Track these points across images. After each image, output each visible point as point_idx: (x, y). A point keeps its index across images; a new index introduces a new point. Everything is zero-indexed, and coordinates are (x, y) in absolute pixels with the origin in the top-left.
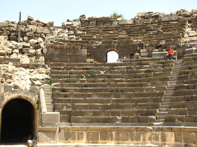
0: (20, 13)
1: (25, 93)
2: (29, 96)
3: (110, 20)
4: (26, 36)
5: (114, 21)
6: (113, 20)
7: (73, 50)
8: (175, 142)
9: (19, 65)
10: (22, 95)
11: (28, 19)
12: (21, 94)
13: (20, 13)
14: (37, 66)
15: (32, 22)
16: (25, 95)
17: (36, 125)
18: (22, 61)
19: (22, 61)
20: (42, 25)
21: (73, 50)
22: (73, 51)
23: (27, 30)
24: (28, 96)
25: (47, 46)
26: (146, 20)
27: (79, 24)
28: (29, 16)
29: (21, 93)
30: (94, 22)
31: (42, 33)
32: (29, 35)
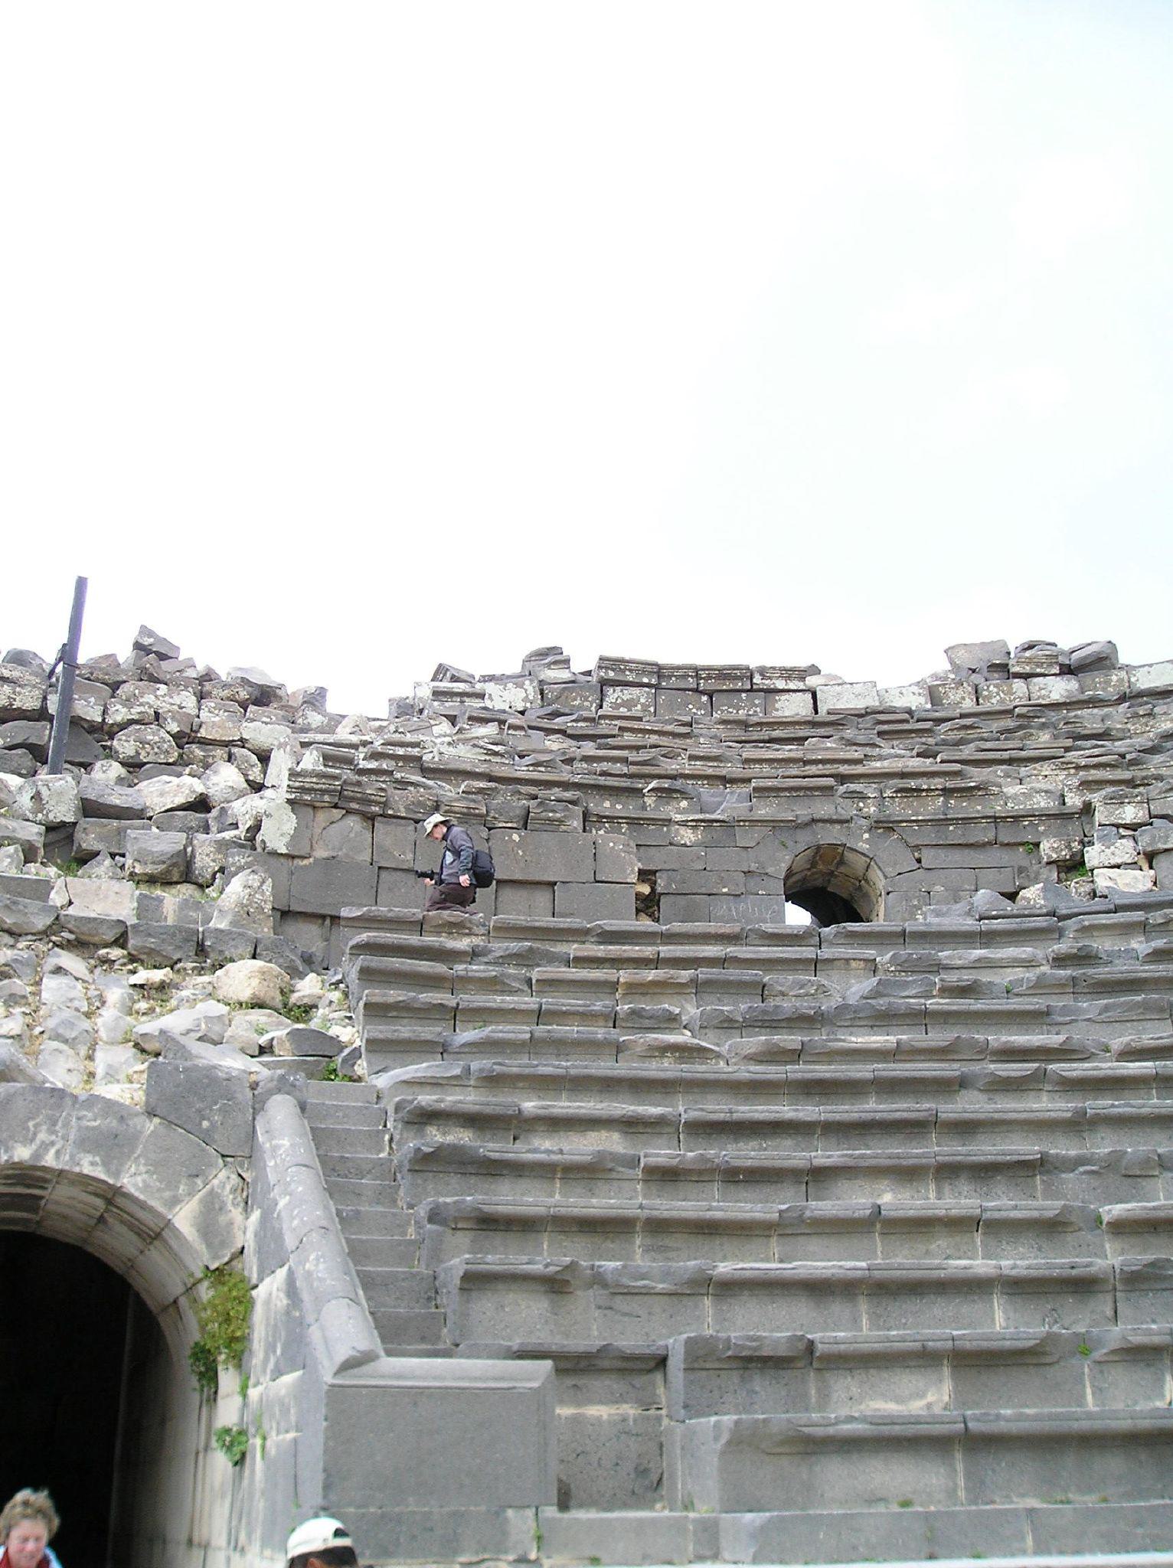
0: (81, 584)
1: (90, 1142)
2: (133, 1180)
3: (757, 679)
4: (110, 753)
5: (789, 691)
6: (780, 684)
7: (516, 837)
8: (192, 1344)
9: (41, 922)
10: (49, 1160)
11: (138, 646)
12: (45, 1146)
13: (81, 584)
14: (201, 950)
15: (165, 665)
16: (89, 1166)
17: (177, 1531)
18: (71, 903)
19: (71, 903)
20: (243, 695)
21: (516, 837)
22: (519, 845)
23: (119, 713)
24: (117, 1174)
25: (303, 790)
26: (1018, 685)
27: (526, 699)
28: (145, 631)
29: (42, 1136)
30: (636, 691)
31: (243, 743)
32: (132, 753)
